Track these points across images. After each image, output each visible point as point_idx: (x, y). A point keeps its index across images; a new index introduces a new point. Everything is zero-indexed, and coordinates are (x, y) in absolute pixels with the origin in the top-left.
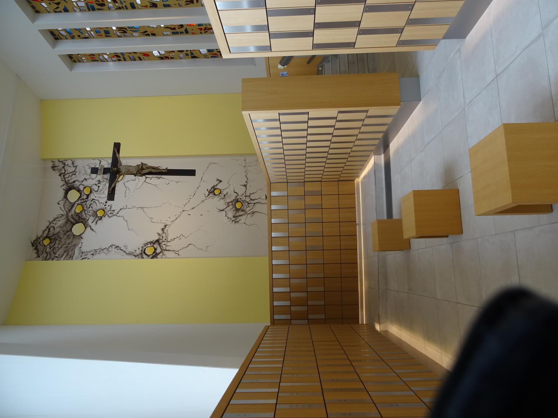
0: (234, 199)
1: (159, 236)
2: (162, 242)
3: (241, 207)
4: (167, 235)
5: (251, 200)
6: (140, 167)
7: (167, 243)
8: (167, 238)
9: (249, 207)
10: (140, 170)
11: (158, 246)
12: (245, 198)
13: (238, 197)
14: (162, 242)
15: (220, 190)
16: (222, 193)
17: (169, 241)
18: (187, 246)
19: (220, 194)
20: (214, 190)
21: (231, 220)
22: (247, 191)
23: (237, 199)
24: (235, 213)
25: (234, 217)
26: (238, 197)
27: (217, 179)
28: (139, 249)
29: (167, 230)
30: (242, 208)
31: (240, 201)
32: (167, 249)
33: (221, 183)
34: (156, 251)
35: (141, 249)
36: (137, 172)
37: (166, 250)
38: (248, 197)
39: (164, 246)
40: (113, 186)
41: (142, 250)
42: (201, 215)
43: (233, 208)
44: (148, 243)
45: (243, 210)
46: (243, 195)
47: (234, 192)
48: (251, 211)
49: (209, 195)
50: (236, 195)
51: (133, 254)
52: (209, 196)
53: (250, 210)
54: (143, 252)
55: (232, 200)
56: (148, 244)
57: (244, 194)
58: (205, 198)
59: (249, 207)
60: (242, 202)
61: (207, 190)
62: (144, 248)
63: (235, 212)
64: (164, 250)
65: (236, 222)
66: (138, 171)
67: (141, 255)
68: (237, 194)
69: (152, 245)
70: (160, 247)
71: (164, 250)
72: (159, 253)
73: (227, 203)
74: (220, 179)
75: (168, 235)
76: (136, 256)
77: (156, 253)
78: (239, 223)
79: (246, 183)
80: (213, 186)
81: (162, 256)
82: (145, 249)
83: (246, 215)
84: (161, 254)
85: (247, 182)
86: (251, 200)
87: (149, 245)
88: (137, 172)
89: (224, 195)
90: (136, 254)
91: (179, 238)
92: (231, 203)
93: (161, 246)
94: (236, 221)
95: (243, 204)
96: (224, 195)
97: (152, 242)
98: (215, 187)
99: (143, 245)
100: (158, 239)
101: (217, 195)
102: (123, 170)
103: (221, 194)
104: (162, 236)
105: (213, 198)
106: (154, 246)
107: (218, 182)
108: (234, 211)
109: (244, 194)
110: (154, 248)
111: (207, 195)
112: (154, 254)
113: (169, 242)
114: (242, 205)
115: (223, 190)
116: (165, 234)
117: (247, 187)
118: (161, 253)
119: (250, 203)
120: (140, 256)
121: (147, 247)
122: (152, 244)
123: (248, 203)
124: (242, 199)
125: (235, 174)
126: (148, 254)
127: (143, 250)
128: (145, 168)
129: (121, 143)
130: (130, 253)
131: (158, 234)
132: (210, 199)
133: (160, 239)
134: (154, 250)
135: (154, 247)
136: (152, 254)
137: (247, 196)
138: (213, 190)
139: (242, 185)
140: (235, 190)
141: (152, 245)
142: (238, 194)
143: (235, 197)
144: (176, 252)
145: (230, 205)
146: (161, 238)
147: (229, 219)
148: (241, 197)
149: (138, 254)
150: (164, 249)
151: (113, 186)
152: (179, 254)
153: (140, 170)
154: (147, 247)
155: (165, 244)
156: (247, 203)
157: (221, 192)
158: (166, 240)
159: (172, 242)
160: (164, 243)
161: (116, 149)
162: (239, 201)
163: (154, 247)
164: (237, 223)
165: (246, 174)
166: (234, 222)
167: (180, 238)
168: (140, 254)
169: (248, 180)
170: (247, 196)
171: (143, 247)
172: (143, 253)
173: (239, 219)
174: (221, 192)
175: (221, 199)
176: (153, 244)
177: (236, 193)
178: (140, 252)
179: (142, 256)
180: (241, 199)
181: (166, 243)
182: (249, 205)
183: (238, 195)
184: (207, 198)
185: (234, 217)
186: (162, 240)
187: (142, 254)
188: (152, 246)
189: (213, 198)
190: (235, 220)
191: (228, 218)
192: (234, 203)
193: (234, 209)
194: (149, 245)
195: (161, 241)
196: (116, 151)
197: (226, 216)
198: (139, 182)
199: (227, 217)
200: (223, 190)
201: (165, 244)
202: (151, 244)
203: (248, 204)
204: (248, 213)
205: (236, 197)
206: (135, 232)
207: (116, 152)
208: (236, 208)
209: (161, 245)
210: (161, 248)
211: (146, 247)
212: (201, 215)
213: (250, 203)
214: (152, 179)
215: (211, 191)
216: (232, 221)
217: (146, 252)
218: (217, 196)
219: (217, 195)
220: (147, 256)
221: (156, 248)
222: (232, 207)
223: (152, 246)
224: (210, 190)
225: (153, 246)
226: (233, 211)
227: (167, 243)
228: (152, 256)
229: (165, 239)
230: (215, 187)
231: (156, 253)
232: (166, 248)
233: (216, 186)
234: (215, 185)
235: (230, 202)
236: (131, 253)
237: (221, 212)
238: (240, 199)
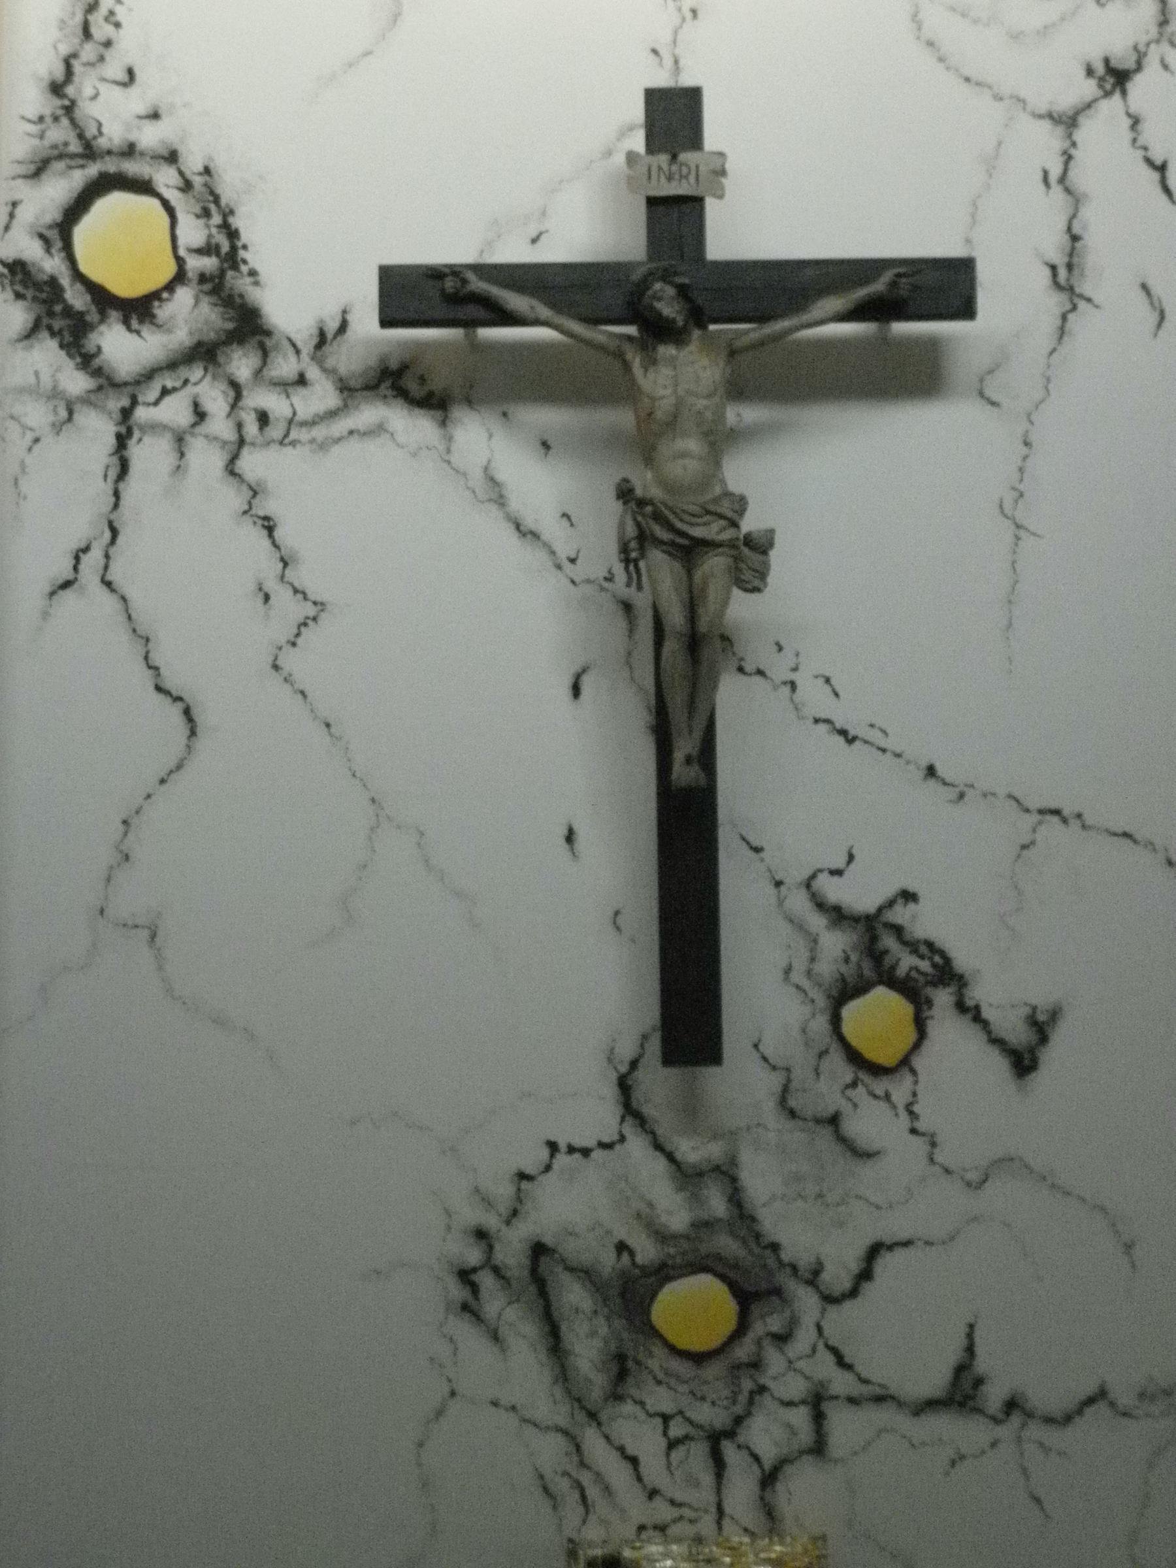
0: (775, 1247)
1: (307, 344)
2: (236, 387)
3: (674, 1350)
4: (319, 432)
5: (769, 1479)
6: (698, 532)
7: (212, 439)
8: (275, 431)
9: (672, 1445)
10: (671, 528)
11: (181, 337)
12: (795, 1387)
13: (807, 1301)
14: (236, 387)
15: (905, 1062)
16: (860, 1092)
17: (252, 463)
18: (168, 684)
19: (855, 1057)
20: (909, 989)
21: (492, 1222)
22: (883, 1415)
23: (778, 1292)
24: (586, 1274)
25: (539, 1250)
26: (807, 1301)
27: (1055, 1015)
28: (155, 116)
29: (379, 429)
30: (658, 1360)
31: (758, 1328)
32: (137, 452)
33: (999, 1065)
34: (114, 315)
35: (150, 137)
36: (650, 502)
37: (122, 441)
38: (806, 1436)
39: (175, 411)
40: (516, 302)
41: (130, 151)
42: (570, 837)
43: (662, 1236)
44: (228, 213)
45: (622, 1375)
46: (842, 1362)
47: (875, 1251)
48: (618, 1474)
49: (838, 915)
50: (837, 1277)
51: (89, 52)
52: (817, 922)
53: (634, 1461)
54: (111, 166)
55: (771, 1223)
56: (206, 213)
57: (841, 1383)
58: (795, 875)
59: (672, 1445)
60: (743, 1351)
61: (908, 896)
62: (165, 179)
63: (608, 1261)
64: (126, 413)
65: (474, 1288)
66: (657, 517)
67: (75, 147)
68: (847, 1285)
69: (195, 264)
70: (172, 365)
71: (126, 413)
72: (87, 361)
73: (733, 1161)
74: (1054, 1056)
75: (322, 446)
76: (56, 89)
77: (93, 317)
78: (463, 1329)
79: (994, 1395)
80: (962, 960)
81: (55, 394)
82: (143, 187)
83: (561, 1415)
84: (77, 382)
85: (1016, 1419)
86: (769, 1479)
87: (192, 232)
88: (649, 509)
89: (834, 1120)
90: (85, 85)
91: (271, 585)
92: (717, 1204)
93: (184, 372)
94: (486, 1280)
95: (713, 1370)
96: (834, 1120)
97: (232, 260)
98: (943, 998)
99: (193, 163)
100: (268, 333)
101: (836, 1021)
102: (665, 372)
103: (847, 1073)
104: (302, 380)
105: (797, 977)
106: (184, 296)
107: (1017, 1033)
108: (621, 1247)
109: (841, 1383)
110: (155, 296)
111: (834, 891)
112: (76, 298)
113: (234, 458)
114: (699, 1358)
115: (900, 1095)
116: (332, 414)
117: (943, 1424)
118: (98, 372)
119: (719, 1464)
120: (60, 133)
121: (166, 205)
122: (209, 263)
123: (730, 1434)
124: (774, 1360)
125: (1128, 1247)
126: (82, 233)
127: (132, 168)
128: (698, 575)
129: (750, 501)
130: (97, 19)
131: (332, 326)
132: (785, 929)
133: (265, 354)
134: (124, 286)
135: (170, 287)
136: (79, 276)
137: (819, 1417)
138: (906, 962)
139: (970, 1350)
140: (900, 1255)
141: (195, 264)
142: (853, 1293)
143: (805, 1260)
144: (92, 560)
145: (696, 1199)
146: (285, 366)
147: (504, 1191)
148: (804, 1338)
149: (89, 110)
150: (142, 414)
151: (516, 302)
152: (68, 595)
153: (671, 528)
154: (166, 205)
155: (200, 415)
156: (709, 1415)
157: (878, 1070)
158: (251, 428)
159: (232, 498)
160: (215, 400)
161: (893, 284)
162: (756, 1309)
163: (170, 287)
164: (458, 1292)
165: (1125, 1400)
166: (473, 1256)
167: (282, 596)
168: (91, 131)
169: (1054, 1437)
170: (819, 1417)
171: (172, 157)
172: (93, 170)
173: (512, 1314)
174: (878, 1070)
175: (775, 1081)
176: (203, 278)
177: (865, 1274)
178: (113, 134)
179: (59, 166)
180: (782, 1339)
181: (220, 425)
182: (699, 1451)
183: (830, 1299)
184: (799, 902)
185: (539, 1250)
186: (258, 373)
187: (90, 152)
188: (180, 261)
189: (797, 977)
190: (496, 1271)
191: (523, 1176)
192: (727, 1245)
193: (647, 1251)
194: (192, 232)
195: (242, 364)
196: (879, 286)
197: (553, 1147)
198: (1016, 36)
199: (532, 1158)
200: (900, 1095)
201: (200, 415)
202: (207, 250)
203: (715, 1439)
204: (592, 1439)
205: (813, 1277)
206: (368, 53)
207: (862, 293)
208: (663, 1273)
209: (196, 372)
210: (149, 375)
211: (172, 195)
212: (570, 837)
213: (719, 1464)
214: (1057, 190)
215: (889, 942)
216: (481, 1234)
217: (114, 203)
218: (821, 1024)
219: (836, 1021)
220: (53, 214)
221: (163, 312)
222: (677, 1217)
223: (180, 261)
224: (898, 930)
225: (180, 277)
226: (621, 1233)
227: (212, 439)
228: (53, 282)
229: (263, 418)
230: (943, 998)
231: (93, 317)
232: (155, 428)
233: (961, 1007)
234: (977, 994)
235: (736, 1198)
236: (101, 30)
237: (610, 1091)
238: (775, 1324)
